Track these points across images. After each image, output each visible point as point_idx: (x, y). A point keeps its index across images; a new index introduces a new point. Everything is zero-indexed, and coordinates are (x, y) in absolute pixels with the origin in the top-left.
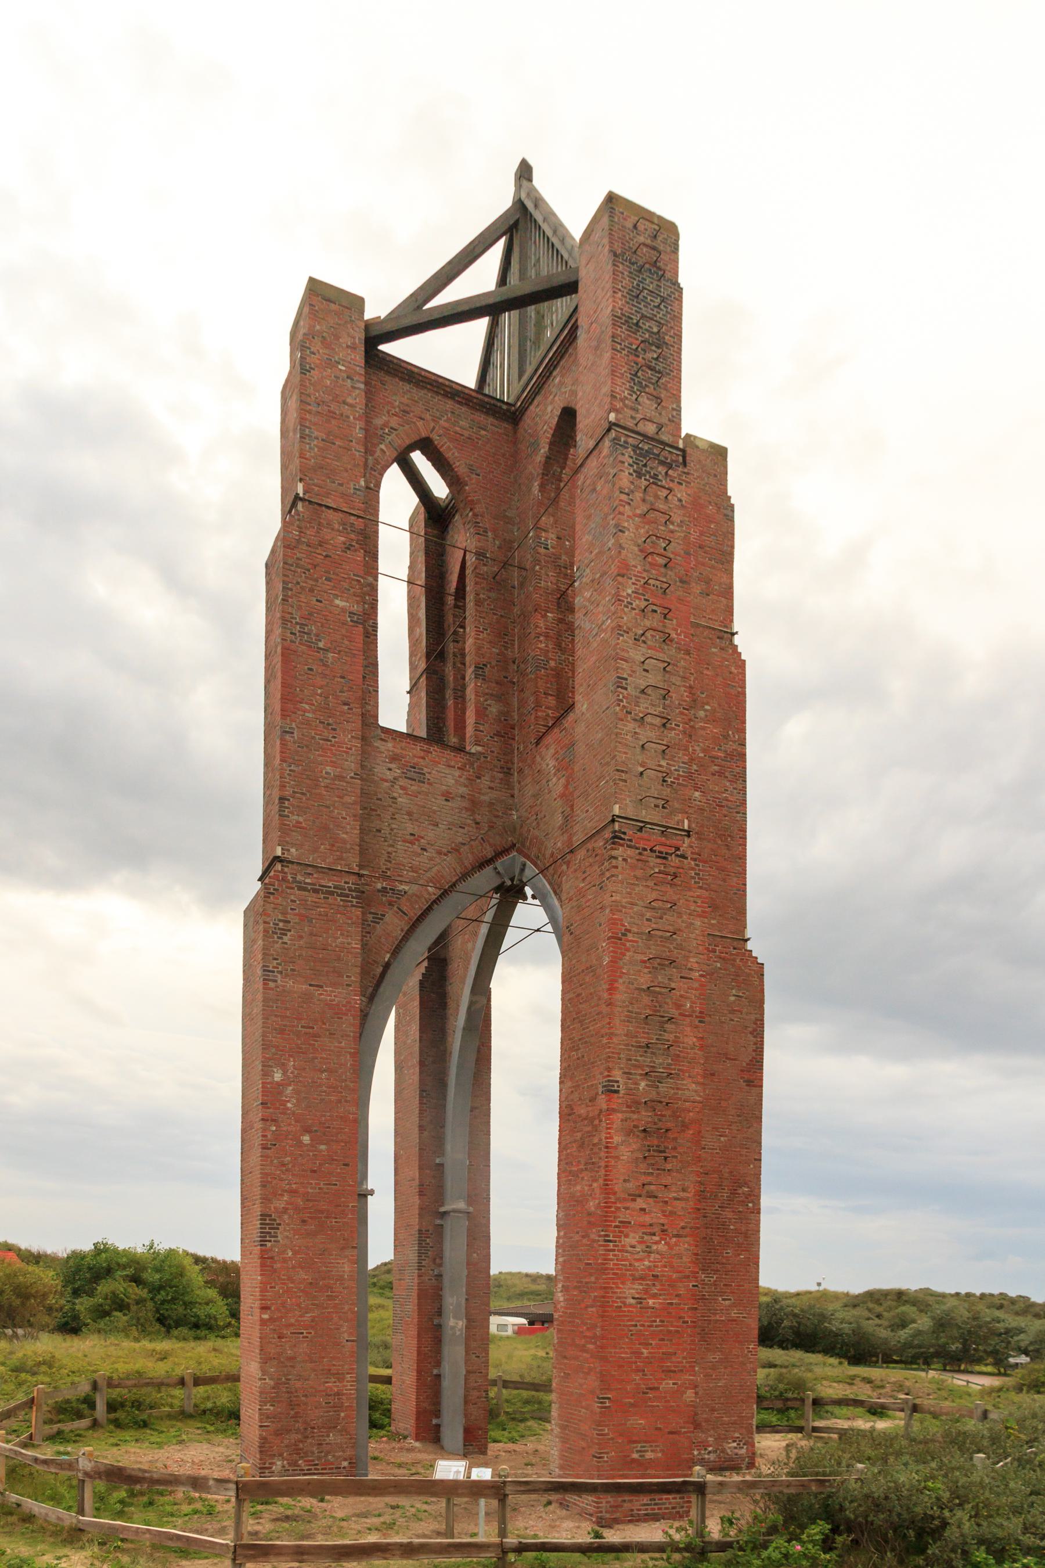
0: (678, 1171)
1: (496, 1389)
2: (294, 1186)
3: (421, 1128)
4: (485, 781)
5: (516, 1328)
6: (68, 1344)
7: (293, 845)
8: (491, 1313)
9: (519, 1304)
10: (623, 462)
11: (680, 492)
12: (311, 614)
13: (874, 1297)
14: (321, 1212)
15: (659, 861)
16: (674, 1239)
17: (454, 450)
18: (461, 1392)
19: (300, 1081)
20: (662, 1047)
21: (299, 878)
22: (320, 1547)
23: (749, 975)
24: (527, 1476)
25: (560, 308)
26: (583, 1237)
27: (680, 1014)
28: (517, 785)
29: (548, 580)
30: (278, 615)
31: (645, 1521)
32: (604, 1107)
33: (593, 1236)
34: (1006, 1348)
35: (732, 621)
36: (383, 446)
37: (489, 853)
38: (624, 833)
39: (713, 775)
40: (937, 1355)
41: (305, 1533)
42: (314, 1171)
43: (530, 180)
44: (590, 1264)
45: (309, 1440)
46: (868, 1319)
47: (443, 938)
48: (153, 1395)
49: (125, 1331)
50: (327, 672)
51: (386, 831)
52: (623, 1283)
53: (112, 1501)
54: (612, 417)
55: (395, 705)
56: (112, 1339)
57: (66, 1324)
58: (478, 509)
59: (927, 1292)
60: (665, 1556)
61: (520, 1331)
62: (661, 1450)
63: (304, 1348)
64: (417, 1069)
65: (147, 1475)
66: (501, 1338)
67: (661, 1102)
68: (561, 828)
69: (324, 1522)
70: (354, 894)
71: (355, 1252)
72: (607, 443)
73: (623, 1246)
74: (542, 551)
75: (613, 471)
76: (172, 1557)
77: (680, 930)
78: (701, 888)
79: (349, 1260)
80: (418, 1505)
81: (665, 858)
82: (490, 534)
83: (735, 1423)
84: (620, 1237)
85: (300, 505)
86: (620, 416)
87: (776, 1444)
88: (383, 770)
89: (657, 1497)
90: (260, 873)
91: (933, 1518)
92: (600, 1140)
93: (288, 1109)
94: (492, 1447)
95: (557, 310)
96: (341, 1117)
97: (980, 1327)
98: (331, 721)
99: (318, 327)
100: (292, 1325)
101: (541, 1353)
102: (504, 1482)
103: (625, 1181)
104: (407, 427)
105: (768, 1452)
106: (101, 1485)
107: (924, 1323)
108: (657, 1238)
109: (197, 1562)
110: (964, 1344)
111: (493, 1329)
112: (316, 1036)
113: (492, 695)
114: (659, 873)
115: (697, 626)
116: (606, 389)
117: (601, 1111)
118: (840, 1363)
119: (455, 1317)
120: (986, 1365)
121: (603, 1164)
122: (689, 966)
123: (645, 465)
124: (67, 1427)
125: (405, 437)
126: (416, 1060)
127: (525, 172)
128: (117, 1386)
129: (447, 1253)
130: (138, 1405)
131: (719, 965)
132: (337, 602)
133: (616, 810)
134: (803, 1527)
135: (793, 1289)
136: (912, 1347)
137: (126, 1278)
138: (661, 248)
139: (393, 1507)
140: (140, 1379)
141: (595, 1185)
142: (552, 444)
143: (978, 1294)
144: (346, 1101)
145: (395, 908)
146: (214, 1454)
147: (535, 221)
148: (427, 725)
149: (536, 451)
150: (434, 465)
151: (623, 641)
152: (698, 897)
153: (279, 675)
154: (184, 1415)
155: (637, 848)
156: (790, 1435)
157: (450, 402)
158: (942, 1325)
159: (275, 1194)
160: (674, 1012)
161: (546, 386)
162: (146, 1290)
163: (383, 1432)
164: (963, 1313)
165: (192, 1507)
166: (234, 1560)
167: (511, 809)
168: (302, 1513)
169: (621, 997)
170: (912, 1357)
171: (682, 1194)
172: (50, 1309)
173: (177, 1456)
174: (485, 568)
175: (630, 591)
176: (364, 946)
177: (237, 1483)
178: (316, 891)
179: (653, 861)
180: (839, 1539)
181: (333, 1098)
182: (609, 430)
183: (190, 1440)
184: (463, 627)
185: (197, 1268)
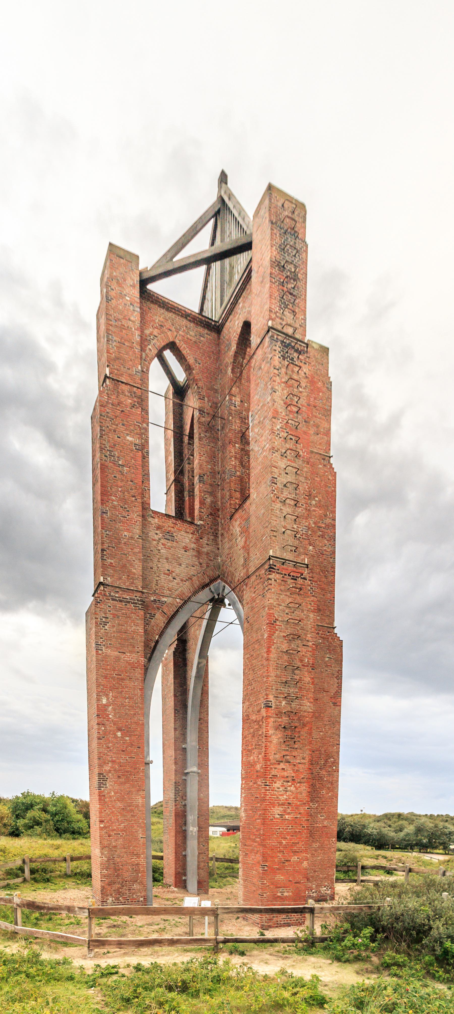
0: (300, 749)
1: (212, 862)
2: (114, 759)
3: (175, 729)
4: (204, 541)
5: (221, 833)
6: (13, 841)
7: (109, 576)
8: (210, 826)
9: (222, 821)
10: (275, 350)
11: (305, 368)
12: (115, 445)
13: (388, 817)
14: (127, 772)
15: (292, 581)
16: (298, 784)
17: (187, 349)
18: (196, 863)
19: (115, 704)
20: (293, 683)
21: (112, 594)
22: (130, 941)
23: (335, 646)
24: (227, 905)
25: (241, 260)
26: (254, 783)
27: (303, 665)
28: (220, 543)
29: (236, 425)
30: (98, 446)
31: (284, 926)
32: (265, 715)
33: (259, 783)
34: (449, 841)
36: (150, 347)
37: (207, 581)
38: (275, 566)
39: (319, 537)
40: (417, 844)
41: (123, 934)
42: (123, 751)
43: (226, 183)
44: (257, 797)
45: (125, 888)
46: (384, 827)
47: (184, 629)
48: (51, 866)
49: (40, 835)
50: (124, 478)
51: (155, 568)
52: (274, 807)
53: (32, 918)
54: (270, 323)
55: (160, 499)
56: (34, 839)
57: (13, 832)
58: (200, 384)
59: (412, 814)
60: (294, 945)
61: (223, 834)
62: (292, 892)
63: (120, 842)
64: (173, 698)
65: (46, 905)
66: (214, 838)
67: (292, 712)
68: (243, 565)
69: (132, 928)
70: (140, 603)
71: (144, 793)
72: (267, 339)
73: (274, 788)
74: (233, 408)
75: (270, 356)
76: (59, 946)
77: (303, 619)
78: (313, 596)
79: (141, 797)
80: (177, 919)
81: (296, 580)
82: (206, 399)
83: (325, 878)
85: (107, 380)
86: (274, 323)
87: (344, 888)
88: (153, 534)
89: (289, 915)
90: (93, 592)
91: (424, 925)
92: (263, 732)
93: (110, 718)
94: (211, 890)
95: (240, 263)
96: (136, 723)
97: (438, 831)
98: (126, 506)
99: (115, 274)
100: (115, 830)
101: (233, 845)
102: (217, 908)
103: (275, 754)
104: (162, 335)
105: (340, 892)
106: (27, 911)
107: (410, 829)
108: (290, 784)
109: (71, 948)
110: (429, 840)
111: (211, 834)
112: (123, 679)
113: (208, 492)
114: (293, 587)
115: (312, 452)
116: (267, 307)
117: (263, 717)
118: (372, 849)
119: (192, 826)
120: (439, 849)
121: (264, 745)
122: (307, 639)
123: (287, 352)
124: (11, 882)
125: (161, 341)
126: (172, 693)
127: (223, 178)
128: (34, 862)
129: (188, 794)
130: (45, 871)
131: (320, 641)
132: (128, 438)
133: (271, 553)
134: (361, 930)
135: (350, 813)
136: (405, 840)
137: (39, 809)
138: (297, 219)
139: (164, 920)
140: (47, 859)
141: (260, 756)
142: (238, 344)
143: (436, 815)
144: (139, 714)
145: (160, 611)
146: (80, 895)
147: (229, 208)
148: (175, 512)
149: (229, 349)
150: (177, 358)
151: (275, 456)
152: (313, 601)
153: (99, 480)
154: (66, 876)
155: (282, 574)
156: (350, 884)
157: (185, 320)
158: (419, 830)
159: (105, 763)
160: (299, 664)
161: (235, 309)
162: (49, 815)
163: (160, 884)
164: (430, 824)
165: (69, 921)
166: (89, 947)
167: (218, 556)
168: (122, 923)
169: (273, 656)
170: (405, 846)
171: (303, 761)
172: (5, 825)
173: (63, 896)
174: (204, 419)
175: (278, 427)
176: (145, 631)
177: (89, 909)
178: (121, 601)
179: (290, 581)
180: (379, 936)
181: (132, 712)
182: (268, 331)
183: (70, 888)
184: (193, 456)
185: (73, 805)
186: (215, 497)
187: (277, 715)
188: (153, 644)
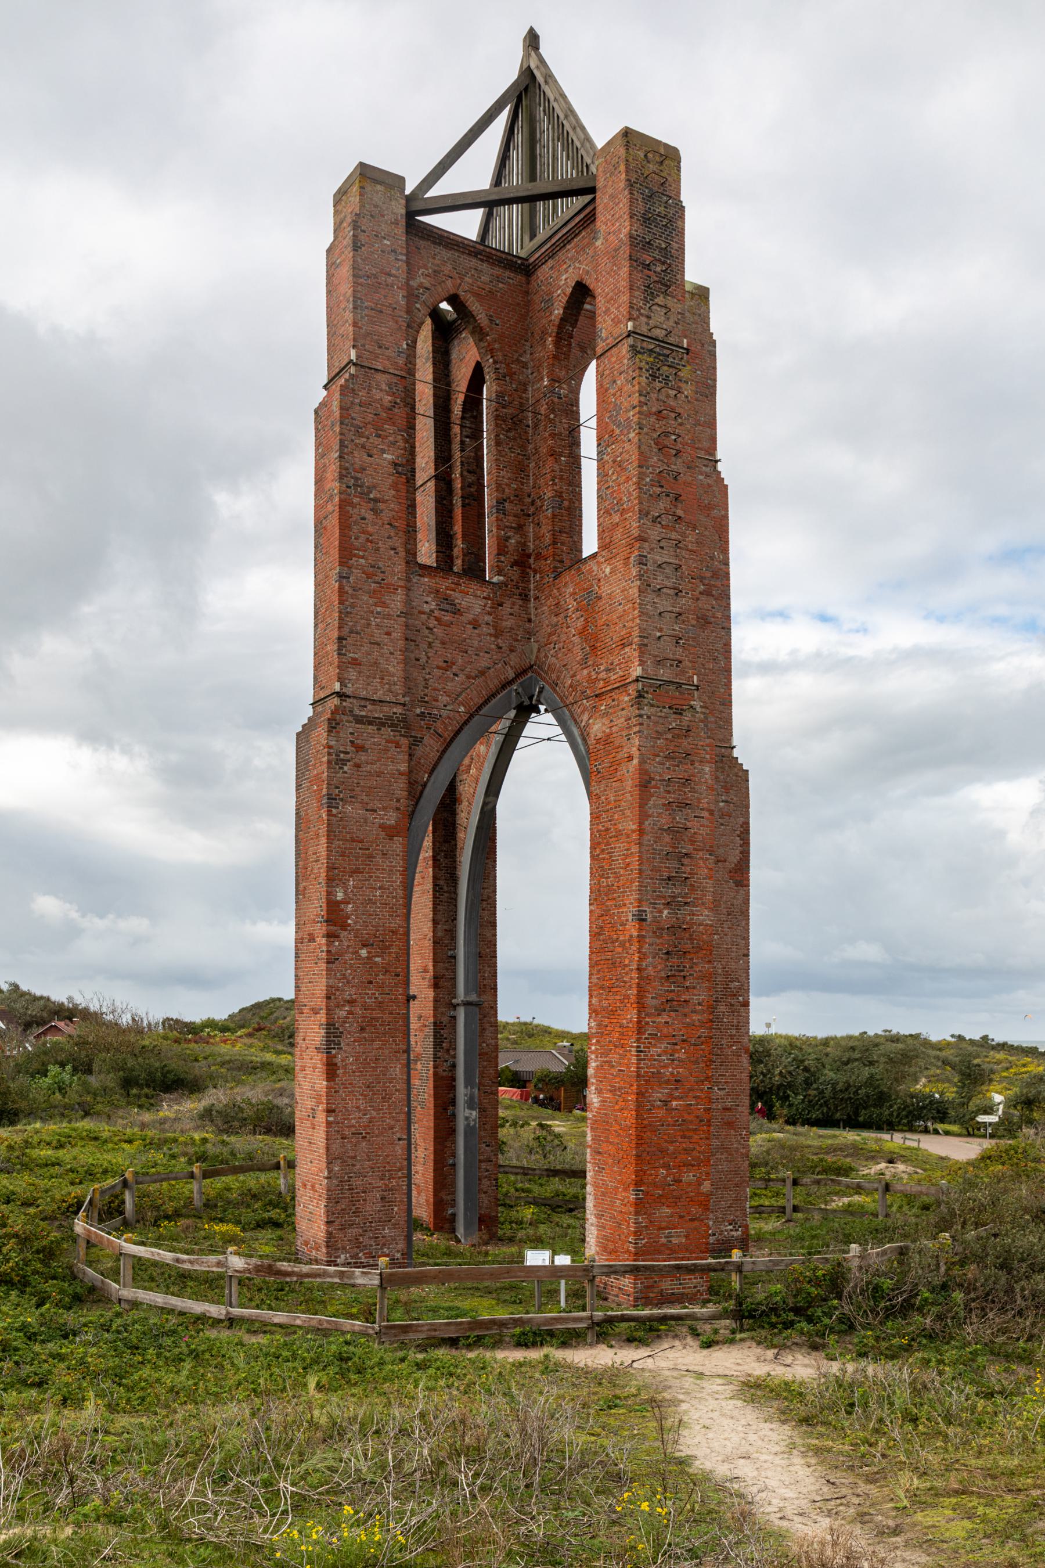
3: (435, 922)
4: (506, 609)
21: (357, 712)
27: (694, 849)
35: (715, 449)
81: (681, 714)
100: (354, 1126)
102: (592, 1266)
108: (678, 1047)
113: (512, 527)
127: (532, 40)
157: (474, 260)
178: (370, 723)
186: (524, 536)
187: (654, 932)
188: (420, 788)
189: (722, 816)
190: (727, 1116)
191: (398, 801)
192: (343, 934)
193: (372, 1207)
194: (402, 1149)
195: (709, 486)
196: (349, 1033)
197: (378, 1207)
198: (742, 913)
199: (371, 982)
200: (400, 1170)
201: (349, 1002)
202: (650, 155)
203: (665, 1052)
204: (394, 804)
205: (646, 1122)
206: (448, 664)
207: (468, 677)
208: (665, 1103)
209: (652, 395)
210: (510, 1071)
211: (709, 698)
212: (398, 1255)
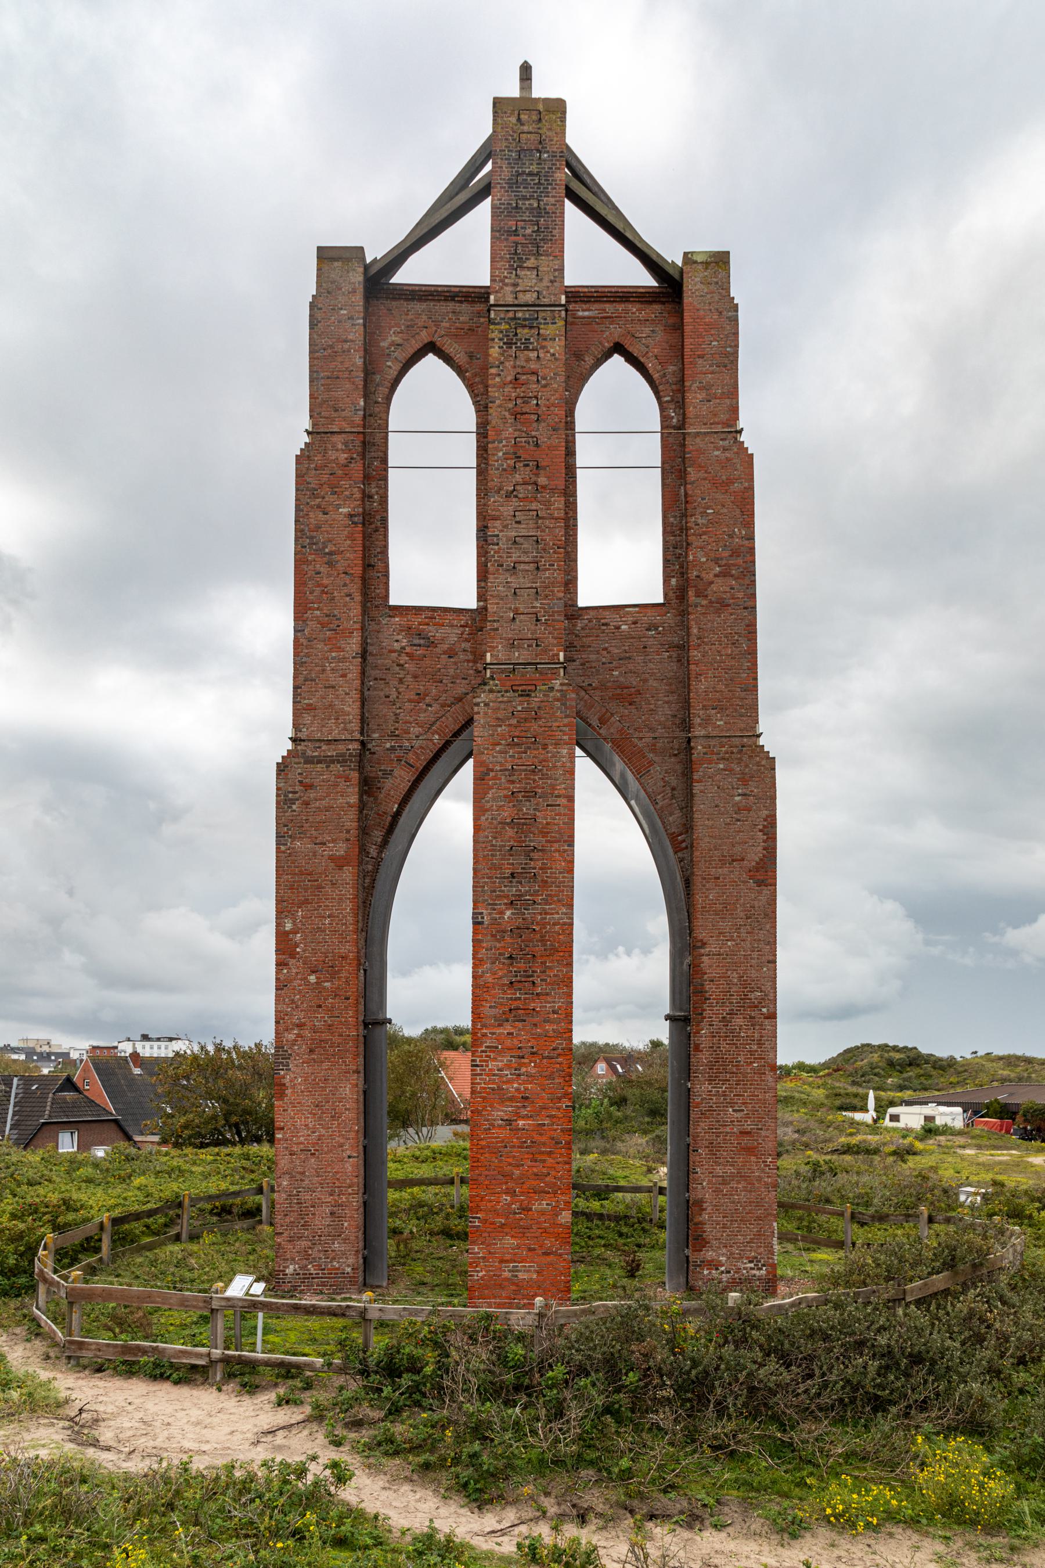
21: (309, 753)
27: (547, 841)
73: (490, 1070)
81: (528, 695)
84: (487, 1061)
100: (302, 1143)
108: (526, 1061)
127: (526, 71)
131: (721, 766)
178: (319, 762)
187: (493, 936)
189: (739, 810)
190: (746, 1141)
191: (348, 832)
192: (292, 962)
193: (321, 1221)
194: (352, 1166)
195: (728, 459)
196: (298, 1054)
197: (328, 1221)
198: (766, 915)
199: (320, 1006)
200: (350, 1187)
201: (298, 1026)
202: (524, 117)
203: (508, 1066)
204: (344, 835)
205: (483, 1143)
206: (420, 696)
207: (443, 706)
208: (509, 1122)
209: (507, 364)
210: (999, 1103)
211: (727, 686)
212: (349, 1270)
